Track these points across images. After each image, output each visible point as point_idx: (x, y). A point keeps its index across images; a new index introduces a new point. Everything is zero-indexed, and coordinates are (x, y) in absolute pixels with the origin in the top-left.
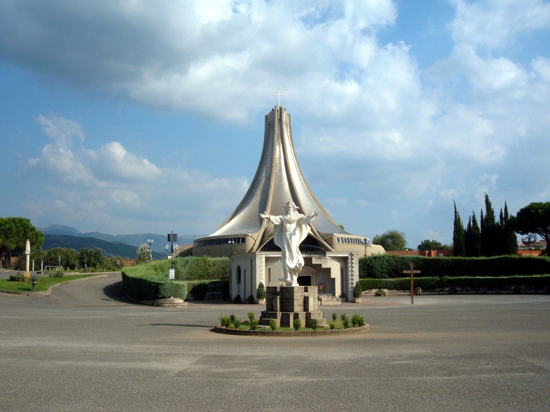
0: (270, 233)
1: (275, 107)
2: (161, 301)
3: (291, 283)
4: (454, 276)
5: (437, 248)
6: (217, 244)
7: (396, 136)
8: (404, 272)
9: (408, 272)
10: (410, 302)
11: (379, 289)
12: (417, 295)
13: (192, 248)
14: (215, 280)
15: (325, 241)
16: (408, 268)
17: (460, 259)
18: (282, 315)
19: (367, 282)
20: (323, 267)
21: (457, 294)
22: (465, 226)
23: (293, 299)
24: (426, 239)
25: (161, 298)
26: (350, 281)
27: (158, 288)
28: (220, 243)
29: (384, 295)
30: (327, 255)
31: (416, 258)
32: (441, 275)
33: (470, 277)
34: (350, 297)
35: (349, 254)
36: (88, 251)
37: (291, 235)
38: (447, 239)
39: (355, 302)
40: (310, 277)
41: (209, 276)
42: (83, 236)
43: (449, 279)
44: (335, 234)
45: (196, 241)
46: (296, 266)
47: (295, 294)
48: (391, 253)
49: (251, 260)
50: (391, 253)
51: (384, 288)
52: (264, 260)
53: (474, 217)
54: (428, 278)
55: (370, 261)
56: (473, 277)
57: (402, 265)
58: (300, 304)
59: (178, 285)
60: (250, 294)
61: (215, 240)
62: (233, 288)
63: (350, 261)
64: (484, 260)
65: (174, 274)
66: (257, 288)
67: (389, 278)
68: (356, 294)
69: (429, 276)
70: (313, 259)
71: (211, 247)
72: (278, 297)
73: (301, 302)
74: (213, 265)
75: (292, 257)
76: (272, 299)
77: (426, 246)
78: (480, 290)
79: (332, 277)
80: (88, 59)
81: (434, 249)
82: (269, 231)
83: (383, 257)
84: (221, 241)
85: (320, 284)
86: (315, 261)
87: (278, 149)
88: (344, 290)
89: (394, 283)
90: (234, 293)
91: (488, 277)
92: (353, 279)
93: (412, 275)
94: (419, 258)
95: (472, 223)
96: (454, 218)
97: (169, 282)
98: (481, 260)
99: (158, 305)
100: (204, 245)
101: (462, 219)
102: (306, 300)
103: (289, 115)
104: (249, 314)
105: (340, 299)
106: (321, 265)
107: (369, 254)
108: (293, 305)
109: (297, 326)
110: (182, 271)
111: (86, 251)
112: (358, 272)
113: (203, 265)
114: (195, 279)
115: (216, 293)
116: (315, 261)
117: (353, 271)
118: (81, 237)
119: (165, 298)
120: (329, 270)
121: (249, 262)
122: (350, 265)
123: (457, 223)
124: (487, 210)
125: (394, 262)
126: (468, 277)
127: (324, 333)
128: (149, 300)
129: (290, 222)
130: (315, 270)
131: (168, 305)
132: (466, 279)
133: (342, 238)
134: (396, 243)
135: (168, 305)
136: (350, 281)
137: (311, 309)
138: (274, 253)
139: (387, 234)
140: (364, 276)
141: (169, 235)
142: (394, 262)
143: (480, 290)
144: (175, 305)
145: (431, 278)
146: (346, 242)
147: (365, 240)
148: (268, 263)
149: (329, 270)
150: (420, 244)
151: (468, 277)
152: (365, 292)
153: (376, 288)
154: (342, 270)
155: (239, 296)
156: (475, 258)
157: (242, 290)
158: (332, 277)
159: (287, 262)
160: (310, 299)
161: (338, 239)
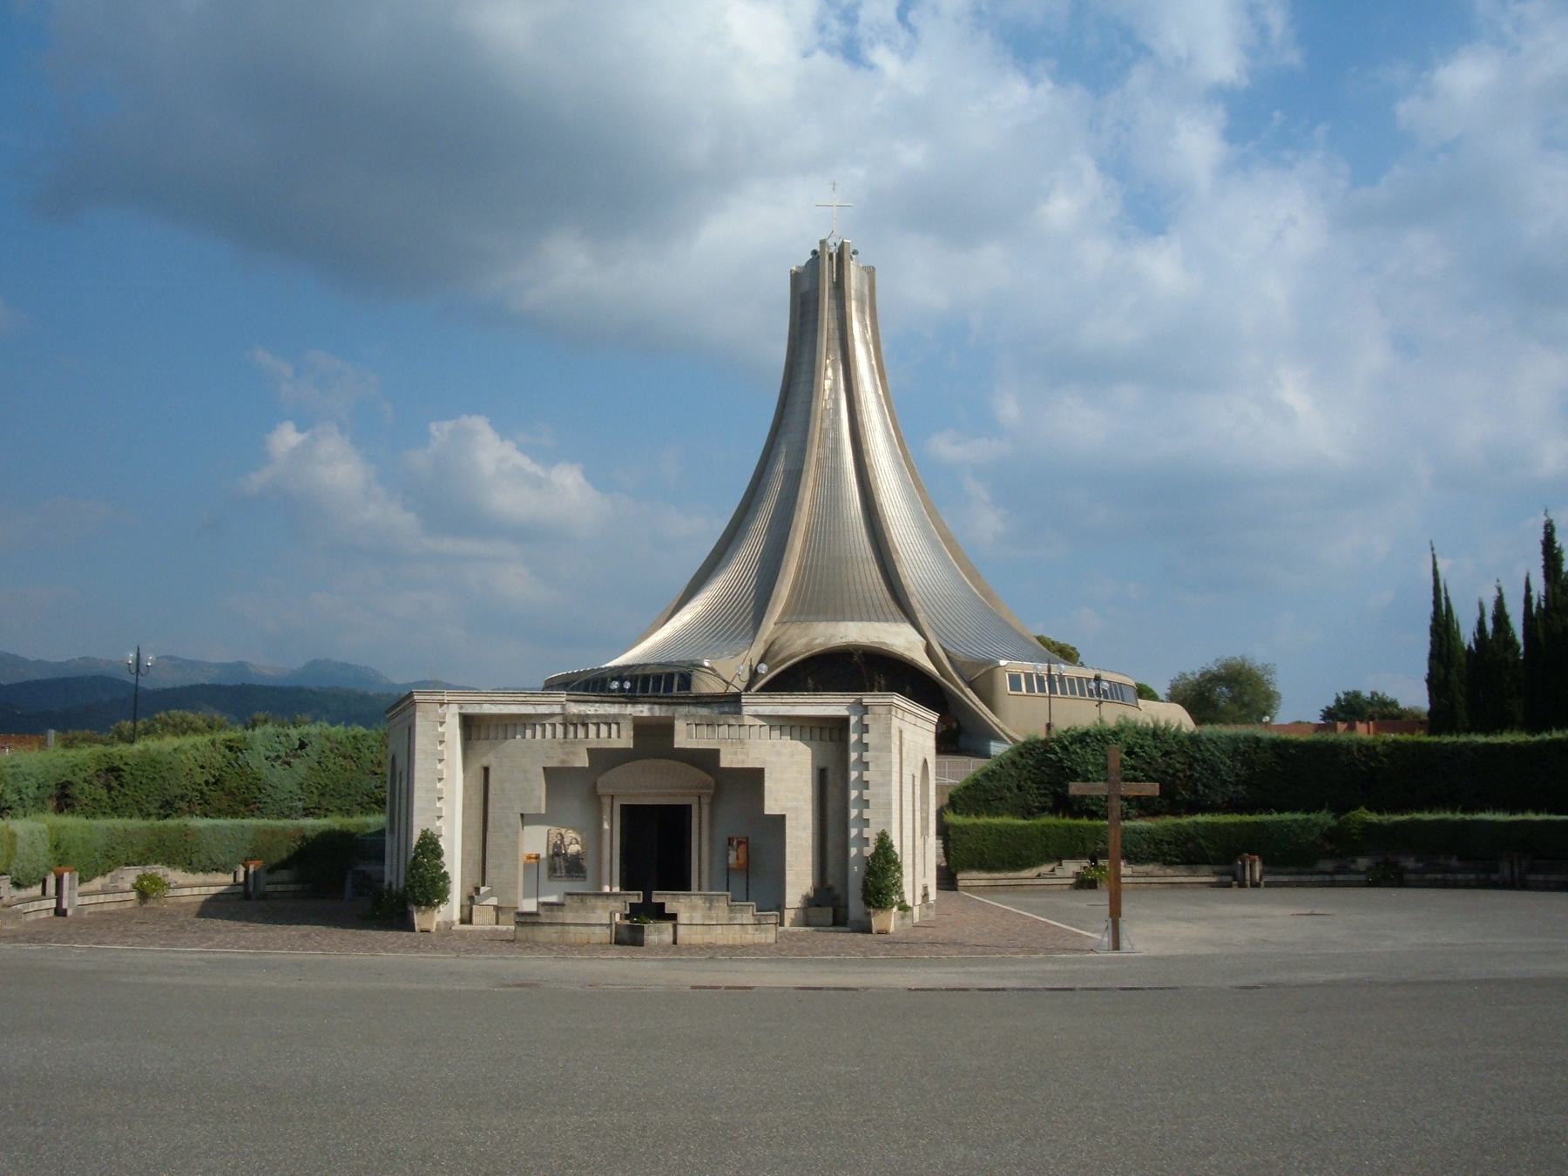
1: (823, 243)
5: (1384, 717)
7: (1294, 393)
9: (1097, 789)
10: (1106, 939)
11: (1094, 859)
12: (1242, 885)
15: (970, 685)
17: (1418, 743)
19: (1044, 831)
20: (726, 762)
22: (1467, 636)
30: (747, 710)
31: (1246, 739)
32: (1340, 808)
33: (1459, 816)
38: (1414, 696)
39: (866, 929)
40: (686, 809)
43: (1371, 825)
44: (1003, 663)
53: (1499, 603)
55: (1064, 748)
56: (1468, 817)
57: (1191, 767)
64: (1516, 749)
67: (1140, 816)
69: (1294, 810)
70: (680, 727)
77: (1350, 709)
79: (771, 807)
80: (423, 199)
82: (778, 653)
83: (1115, 733)
85: (730, 840)
86: (686, 736)
87: (829, 378)
88: (832, 869)
91: (1531, 816)
94: (1258, 740)
95: (1489, 626)
96: (1431, 609)
98: (1503, 746)
101: (1457, 612)
103: (870, 272)
106: (715, 754)
107: (1061, 725)
116: (686, 736)
120: (753, 779)
123: (1442, 625)
124: (1547, 577)
125: (1157, 754)
126: (1448, 816)
130: (710, 780)
140: (1042, 809)
142: (1157, 754)
145: (1300, 816)
147: (1097, 679)
148: (480, 746)
149: (753, 779)
150: (1332, 703)
151: (1448, 816)
152: (1034, 872)
153: (1082, 856)
156: (1481, 739)
158: (771, 807)
161: (1015, 681)
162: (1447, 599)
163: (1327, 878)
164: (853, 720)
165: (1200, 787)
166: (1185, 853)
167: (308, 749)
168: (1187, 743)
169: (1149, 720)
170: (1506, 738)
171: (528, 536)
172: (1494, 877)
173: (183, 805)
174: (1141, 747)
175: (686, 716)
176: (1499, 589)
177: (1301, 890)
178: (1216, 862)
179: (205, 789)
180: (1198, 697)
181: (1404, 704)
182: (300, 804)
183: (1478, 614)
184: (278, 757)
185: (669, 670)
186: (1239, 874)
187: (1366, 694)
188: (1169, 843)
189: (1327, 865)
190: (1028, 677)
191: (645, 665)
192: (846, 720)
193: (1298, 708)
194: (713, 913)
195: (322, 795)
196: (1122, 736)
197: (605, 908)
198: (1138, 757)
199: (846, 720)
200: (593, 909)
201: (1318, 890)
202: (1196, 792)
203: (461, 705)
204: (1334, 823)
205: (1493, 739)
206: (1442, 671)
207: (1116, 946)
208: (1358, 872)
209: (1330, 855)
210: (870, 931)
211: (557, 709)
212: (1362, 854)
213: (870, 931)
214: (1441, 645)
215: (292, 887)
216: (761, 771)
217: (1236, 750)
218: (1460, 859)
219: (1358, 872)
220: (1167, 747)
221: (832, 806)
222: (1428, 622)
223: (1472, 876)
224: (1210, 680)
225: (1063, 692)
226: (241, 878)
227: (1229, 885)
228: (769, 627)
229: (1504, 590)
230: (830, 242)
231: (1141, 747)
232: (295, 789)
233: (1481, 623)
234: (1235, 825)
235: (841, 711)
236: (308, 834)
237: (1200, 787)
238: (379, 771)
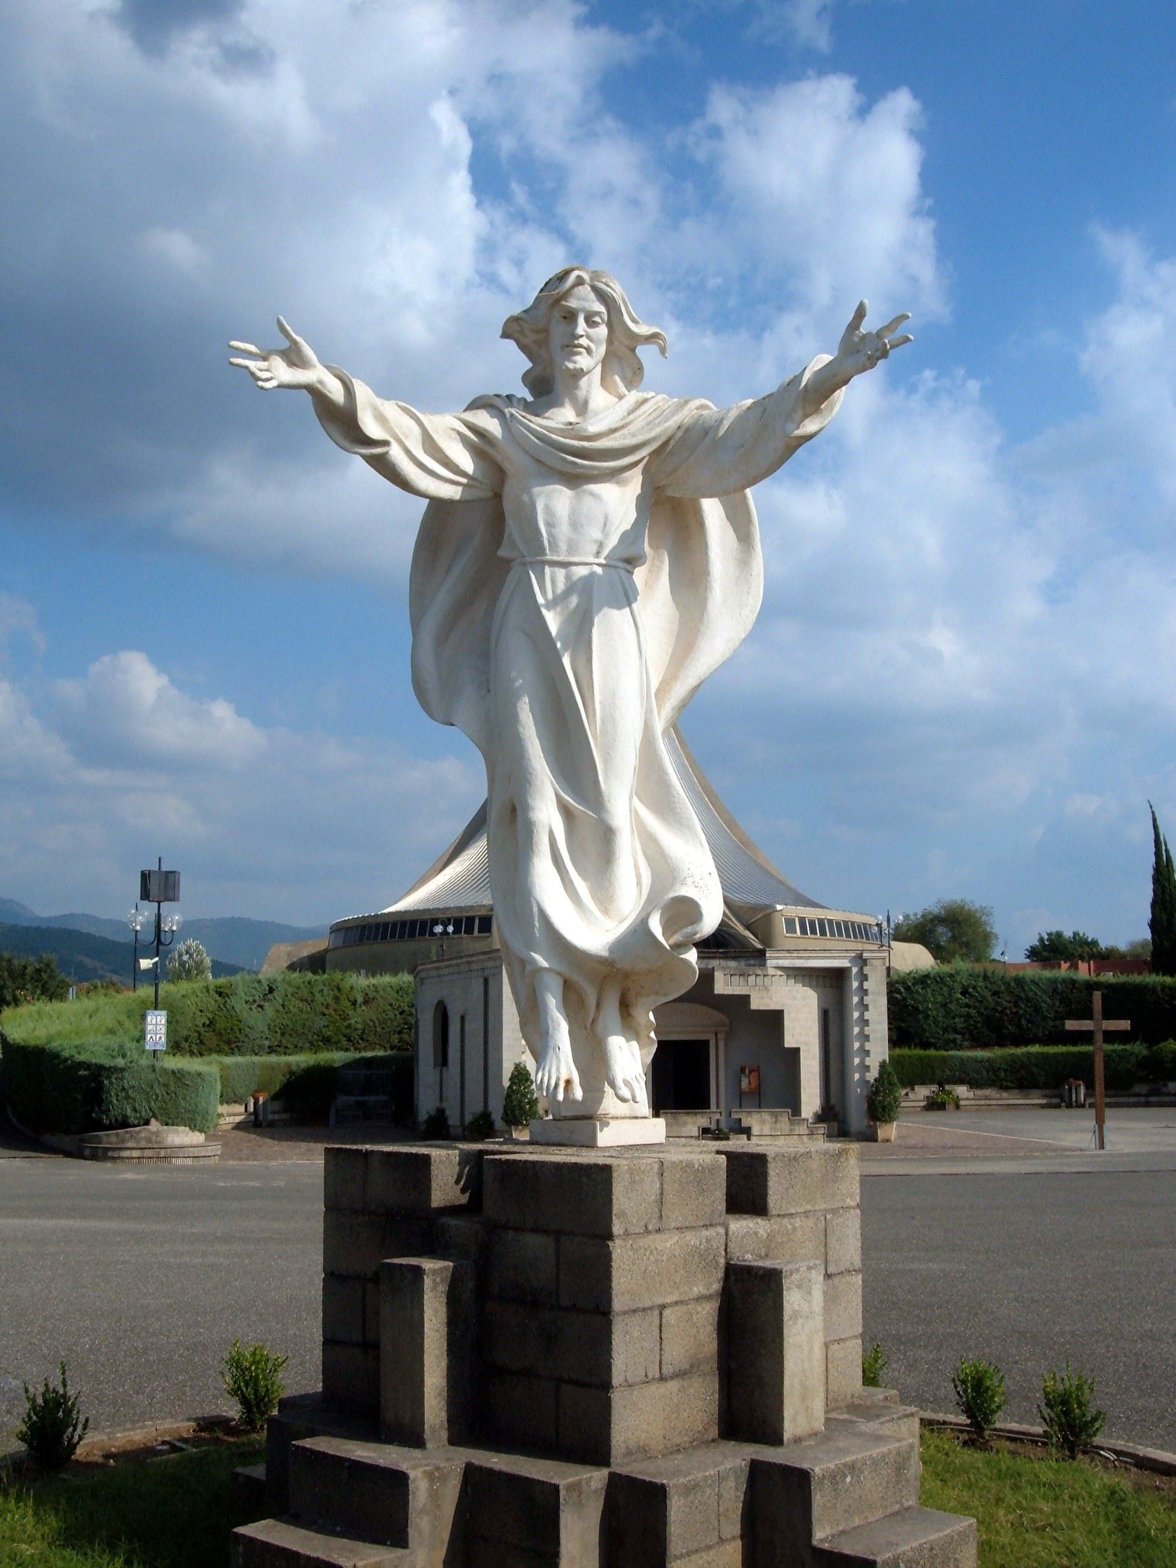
2: (109, 1138)
3: (581, 1121)
6: (402, 936)
7: (944, 641)
8: (1071, 1025)
9: (1086, 1025)
11: (941, 1084)
12: (1069, 1106)
13: (326, 951)
14: (369, 1054)
15: (748, 927)
16: (1087, 1014)
20: (755, 1004)
24: (1054, 930)
25: (111, 1127)
26: (857, 1061)
27: (100, 1084)
28: (412, 935)
29: (958, 1107)
30: (770, 963)
31: (1064, 981)
34: (856, 1116)
35: (853, 960)
36: (16, 962)
37: (586, 603)
39: (873, 1138)
40: (708, 1041)
41: (351, 1041)
42: (44, 926)
44: (779, 907)
45: (338, 929)
46: (641, 929)
47: (619, 1251)
48: (946, 968)
49: (486, 980)
51: (955, 1083)
55: (908, 988)
57: (1016, 1005)
58: (677, 1352)
59: (178, 1075)
60: (479, 1108)
63: (855, 984)
66: (506, 1083)
67: (972, 1047)
68: (880, 1108)
70: (719, 976)
71: (379, 948)
72: (435, 1272)
73: (694, 1329)
74: (366, 1002)
75: (593, 842)
77: (1051, 950)
79: (789, 1042)
84: (414, 926)
85: (743, 1070)
86: (723, 985)
89: (990, 1065)
90: (426, 1103)
92: (867, 1053)
93: (1099, 1037)
99: (99, 1155)
100: (361, 940)
102: (747, 1309)
104: (236, 1363)
105: (822, 1128)
106: (746, 999)
108: (597, 1383)
110: (252, 1022)
111: (9, 961)
113: (329, 1000)
114: (298, 1049)
115: (372, 1099)
117: (866, 1023)
118: (37, 929)
119: (124, 1124)
120: (775, 1019)
121: (478, 988)
122: (856, 999)
125: (987, 994)
129: (577, 465)
131: (135, 1154)
133: (802, 921)
134: (964, 939)
135: (135, 1154)
136: (857, 1061)
137: (803, 1405)
139: (936, 911)
141: (145, 877)
144: (163, 1155)
146: (813, 932)
149: (775, 1019)
153: (931, 1082)
154: (825, 1016)
155: (441, 1112)
157: (452, 1093)
158: (789, 1042)
159: (547, 887)
160: (792, 1300)
161: (790, 923)
162: (1167, 851)
163: (1142, 1099)
164: (855, 970)
165: (1024, 1022)
166: (1020, 1079)
167: (275, 993)
168: (1013, 984)
171: (182, 768)
173: (186, 1045)
174: (975, 988)
175: (724, 969)
177: (1161, 1109)
178: (1046, 1086)
179: (202, 1030)
182: (267, 1043)
184: (255, 1001)
185: (471, 914)
186: (1067, 1094)
188: (1005, 1071)
189: (1141, 1088)
190: (802, 921)
191: (424, 911)
192: (849, 969)
193: (1011, 948)
194: (778, 1126)
195: (283, 1034)
196: (958, 978)
197: (694, 1123)
198: (971, 996)
199: (849, 969)
200: (685, 1123)
201: (1127, 1109)
202: (1020, 1026)
204: (1145, 1052)
206: (1164, 917)
207: (1102, 1147)
208: (1169, 1094)
210: (876, 1141)
213: (876, 1141)
214: (1163, 892)
215: (284, 1116)
216: (782, 1011)
217: (1055, 990)
220: (995, 988)
222: (1150, 872)
224: (932, 921)
225: (832, 934)
226: (251, 1109)
227: (1057, 1106)
232: (265, 1029)
234: (1062, 1054)
235: (844, 963)
236: (294, 1068)
237: (1024, 1022)
238: (327, 1012)
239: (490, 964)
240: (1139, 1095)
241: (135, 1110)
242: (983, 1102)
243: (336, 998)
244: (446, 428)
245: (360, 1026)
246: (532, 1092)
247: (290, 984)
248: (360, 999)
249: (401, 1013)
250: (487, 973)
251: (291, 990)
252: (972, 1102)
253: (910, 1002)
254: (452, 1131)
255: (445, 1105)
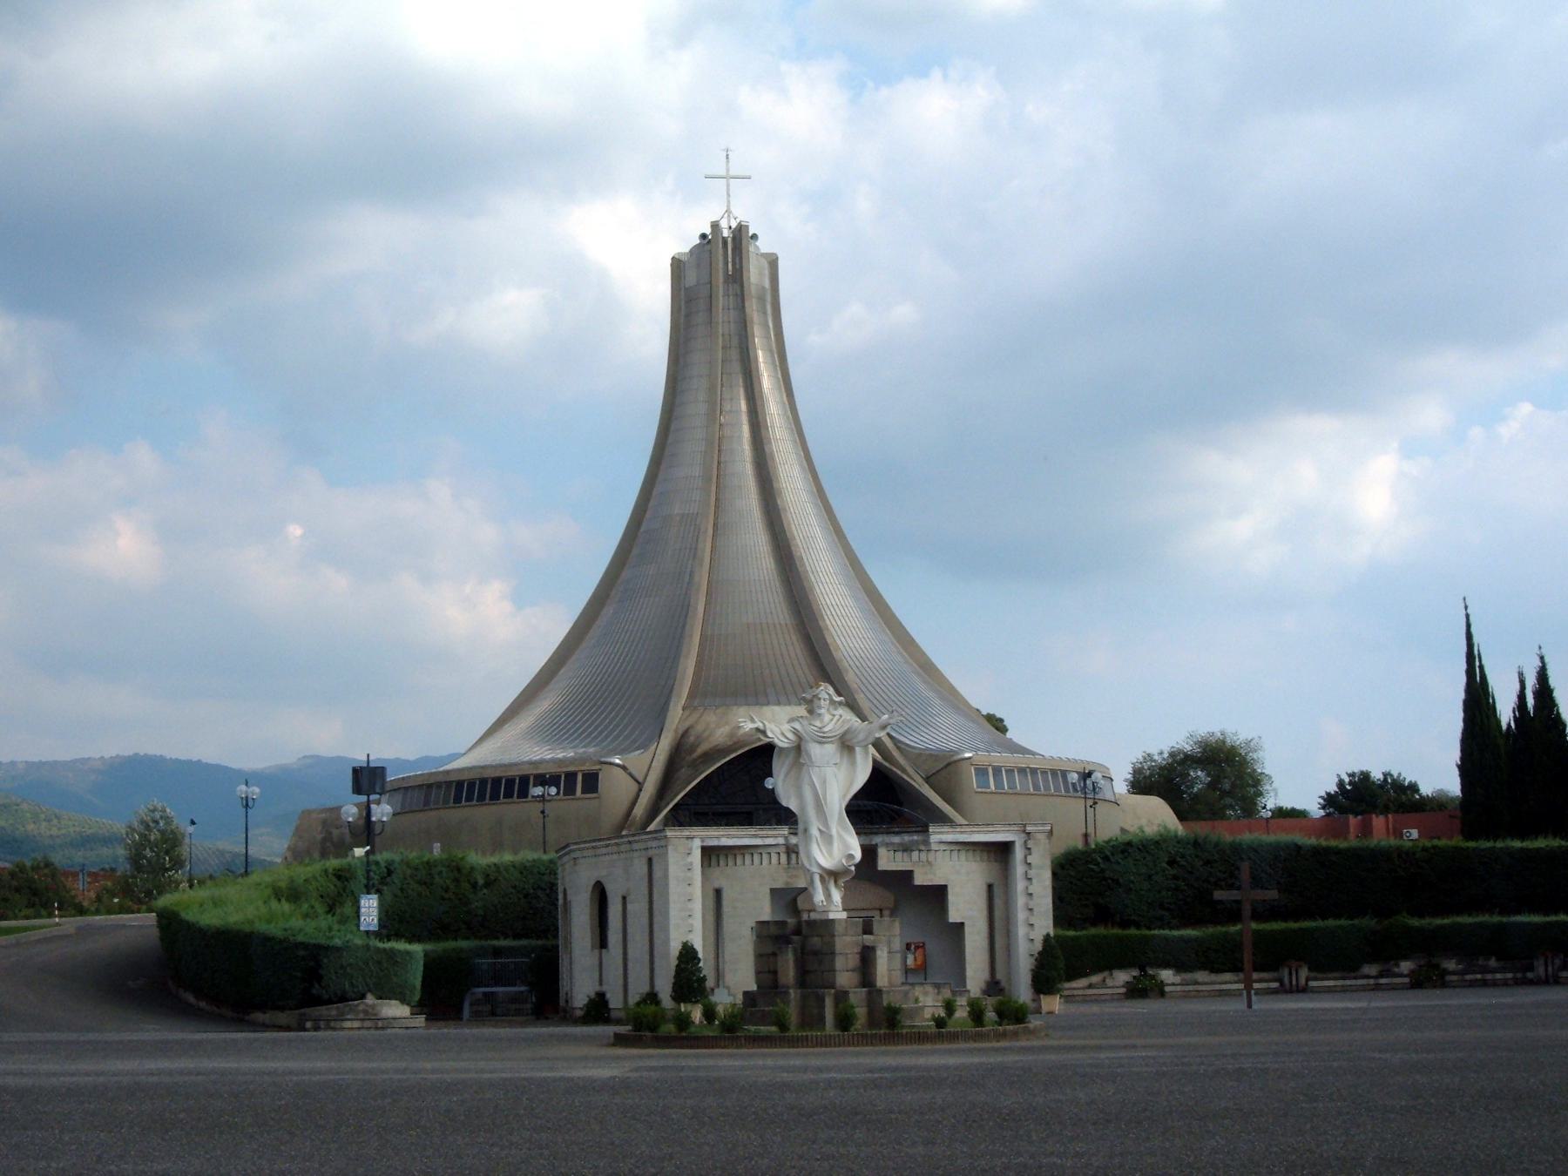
0: (699, 751)
1: (715, 226)
4: (1436, 914)
6: (481, 798)
11: (1142, 969)
16: (1231, 882)
18: (804, 998)
20: (919, 880)
21: (1444, 985)
22: (1506, 712)
23: (833, 953)
28: (495, 797)
29: (1162, 994)
30: (934, 838)
33: (1496, 919)
38: (1437, 771)
49: (650, 860)
50: (1201, 829)
52: (697, 854)
54: (1331, 922)
56: (1505, 919)
59: (391, 954)
60: (646, 989)
61: (471, 784)
62: (577, 968)
65: (375, 912)
69: (1337, 916)
70: (882, 853)
74: (487, 885)
75: (827, 837)
76: (774, 954)
77: (1360, 797)
78: (1531, 968)
79: (954, 916)
81: (1385, 810)
82: (693, 748)
85: (908, 946)
86: (887, 861)
90: (580, 986)
93: (1247, 910)
94: (1298, 848)
96: (1463, 679)
97: (358, 942)
98: (1538, 850)
100: (457, 800)
102: (867, 957)
106: (910, 873)
109: (844, 1021)
112: (1049, 900)
119: (343, 999)
120: (938, 894)
121: (640, 867)
123: (1477, 697)
125: (1198, 863)
127: (920, 1037)
128: (282, 1009)
132: (1481, 925)
137: (882, 980)
138: (733, 831)
142: (1198, 863)
143: (1531, 968)
149: (938, 894)
150: (1333, 788)
152: (1083, 982)
155: (601, 996)
156: (1517, 844)
158: (954, 916)
160: (879, 953)
162: (1481, 667)
163: (1372, 981)
167: (394, 876)
169: (1144, 822)
170: (1540, 843)
172: (1530, 975)
174: (1183, 856)
175: (887, 845)
176: (1542, 658)
180: (1158, 780)
181: (1426, 789)
183: (1517, 686)
185: (571, 769)
187: (1377, 775)
189: (1371, 969)
203: (703, 840)
205: (1528, 844)
208: (1401, 975)
209: (1372, 960)
211: (781, 841)
212: (1406, 958)
218: (1498, 960)
219: (1401, 975)
221: (998, 914)
223: (1510, 975)
228: (676, 717)
229: (1547, 660)
230: (724, 224)
231: (1183, 856)
233: (1522, 697)
234: (1282, 932)
239: (654, 844)
240: (1368, 977)
241: (352, 984)
242: (1191, 988)
243: (457, 880)
244: (786, 727)
245: (481, 912)
246: (700, 970)
247: (408, 864)
248: (481, 882)
249: (526, 896)
250: (651, 853)
251: (409, 872)
252: (1179, 988)
253: (1108, 874)
254: (614, 1015)
255: (604, 988)
